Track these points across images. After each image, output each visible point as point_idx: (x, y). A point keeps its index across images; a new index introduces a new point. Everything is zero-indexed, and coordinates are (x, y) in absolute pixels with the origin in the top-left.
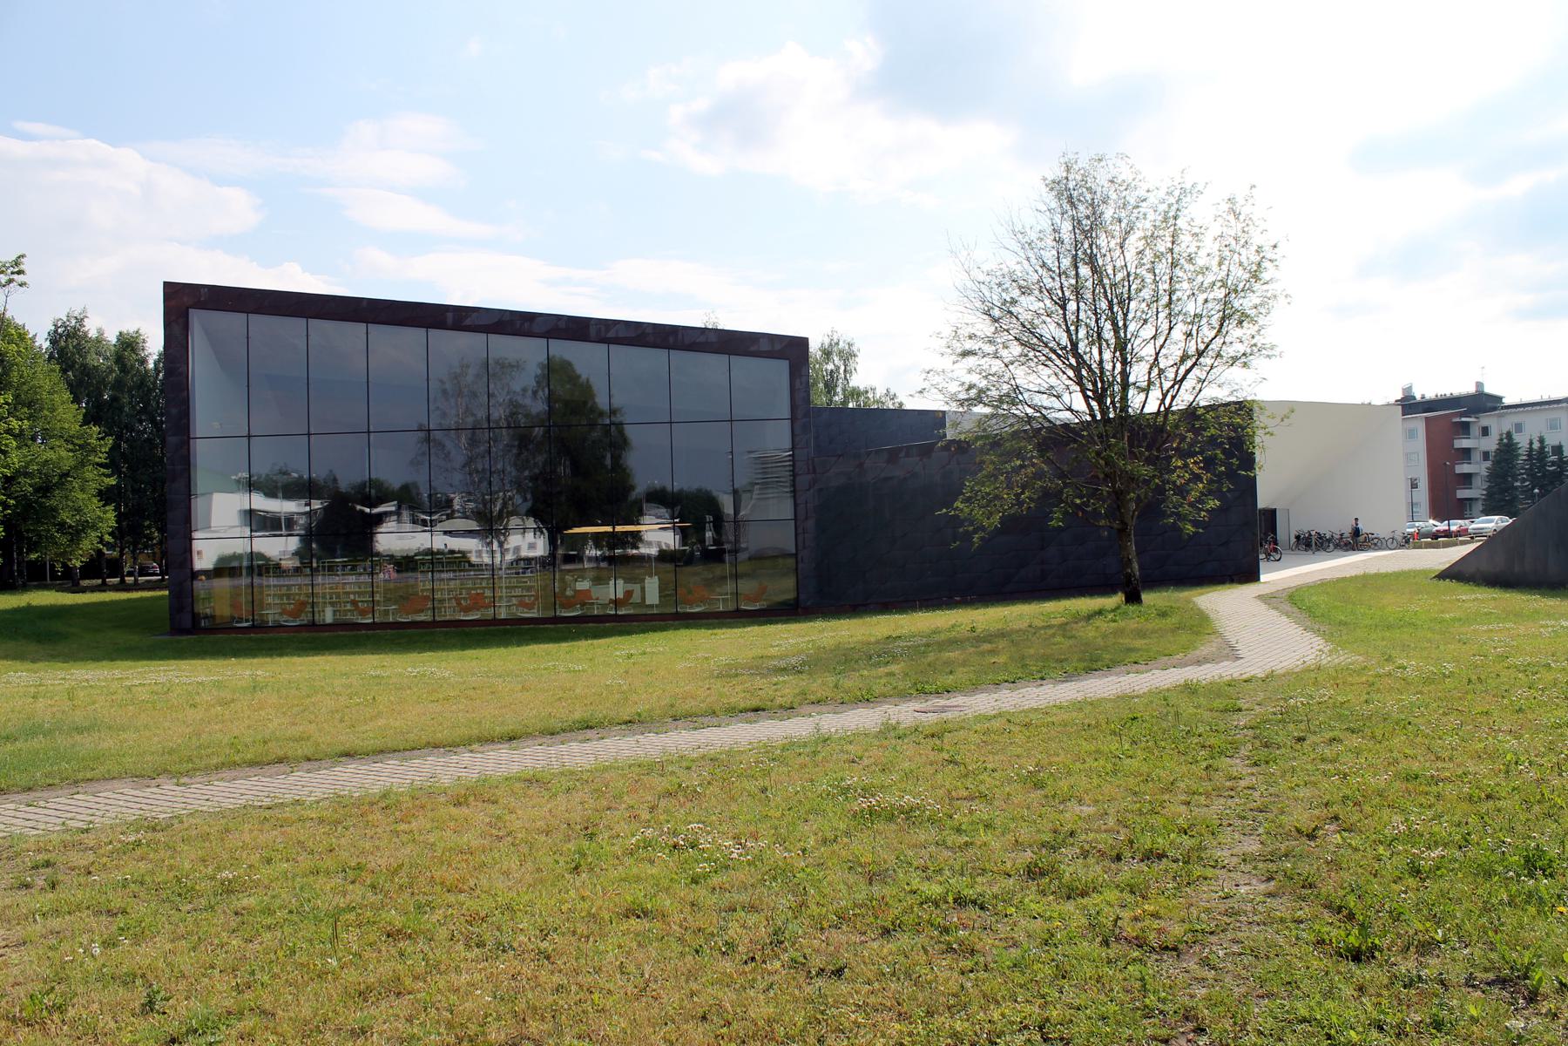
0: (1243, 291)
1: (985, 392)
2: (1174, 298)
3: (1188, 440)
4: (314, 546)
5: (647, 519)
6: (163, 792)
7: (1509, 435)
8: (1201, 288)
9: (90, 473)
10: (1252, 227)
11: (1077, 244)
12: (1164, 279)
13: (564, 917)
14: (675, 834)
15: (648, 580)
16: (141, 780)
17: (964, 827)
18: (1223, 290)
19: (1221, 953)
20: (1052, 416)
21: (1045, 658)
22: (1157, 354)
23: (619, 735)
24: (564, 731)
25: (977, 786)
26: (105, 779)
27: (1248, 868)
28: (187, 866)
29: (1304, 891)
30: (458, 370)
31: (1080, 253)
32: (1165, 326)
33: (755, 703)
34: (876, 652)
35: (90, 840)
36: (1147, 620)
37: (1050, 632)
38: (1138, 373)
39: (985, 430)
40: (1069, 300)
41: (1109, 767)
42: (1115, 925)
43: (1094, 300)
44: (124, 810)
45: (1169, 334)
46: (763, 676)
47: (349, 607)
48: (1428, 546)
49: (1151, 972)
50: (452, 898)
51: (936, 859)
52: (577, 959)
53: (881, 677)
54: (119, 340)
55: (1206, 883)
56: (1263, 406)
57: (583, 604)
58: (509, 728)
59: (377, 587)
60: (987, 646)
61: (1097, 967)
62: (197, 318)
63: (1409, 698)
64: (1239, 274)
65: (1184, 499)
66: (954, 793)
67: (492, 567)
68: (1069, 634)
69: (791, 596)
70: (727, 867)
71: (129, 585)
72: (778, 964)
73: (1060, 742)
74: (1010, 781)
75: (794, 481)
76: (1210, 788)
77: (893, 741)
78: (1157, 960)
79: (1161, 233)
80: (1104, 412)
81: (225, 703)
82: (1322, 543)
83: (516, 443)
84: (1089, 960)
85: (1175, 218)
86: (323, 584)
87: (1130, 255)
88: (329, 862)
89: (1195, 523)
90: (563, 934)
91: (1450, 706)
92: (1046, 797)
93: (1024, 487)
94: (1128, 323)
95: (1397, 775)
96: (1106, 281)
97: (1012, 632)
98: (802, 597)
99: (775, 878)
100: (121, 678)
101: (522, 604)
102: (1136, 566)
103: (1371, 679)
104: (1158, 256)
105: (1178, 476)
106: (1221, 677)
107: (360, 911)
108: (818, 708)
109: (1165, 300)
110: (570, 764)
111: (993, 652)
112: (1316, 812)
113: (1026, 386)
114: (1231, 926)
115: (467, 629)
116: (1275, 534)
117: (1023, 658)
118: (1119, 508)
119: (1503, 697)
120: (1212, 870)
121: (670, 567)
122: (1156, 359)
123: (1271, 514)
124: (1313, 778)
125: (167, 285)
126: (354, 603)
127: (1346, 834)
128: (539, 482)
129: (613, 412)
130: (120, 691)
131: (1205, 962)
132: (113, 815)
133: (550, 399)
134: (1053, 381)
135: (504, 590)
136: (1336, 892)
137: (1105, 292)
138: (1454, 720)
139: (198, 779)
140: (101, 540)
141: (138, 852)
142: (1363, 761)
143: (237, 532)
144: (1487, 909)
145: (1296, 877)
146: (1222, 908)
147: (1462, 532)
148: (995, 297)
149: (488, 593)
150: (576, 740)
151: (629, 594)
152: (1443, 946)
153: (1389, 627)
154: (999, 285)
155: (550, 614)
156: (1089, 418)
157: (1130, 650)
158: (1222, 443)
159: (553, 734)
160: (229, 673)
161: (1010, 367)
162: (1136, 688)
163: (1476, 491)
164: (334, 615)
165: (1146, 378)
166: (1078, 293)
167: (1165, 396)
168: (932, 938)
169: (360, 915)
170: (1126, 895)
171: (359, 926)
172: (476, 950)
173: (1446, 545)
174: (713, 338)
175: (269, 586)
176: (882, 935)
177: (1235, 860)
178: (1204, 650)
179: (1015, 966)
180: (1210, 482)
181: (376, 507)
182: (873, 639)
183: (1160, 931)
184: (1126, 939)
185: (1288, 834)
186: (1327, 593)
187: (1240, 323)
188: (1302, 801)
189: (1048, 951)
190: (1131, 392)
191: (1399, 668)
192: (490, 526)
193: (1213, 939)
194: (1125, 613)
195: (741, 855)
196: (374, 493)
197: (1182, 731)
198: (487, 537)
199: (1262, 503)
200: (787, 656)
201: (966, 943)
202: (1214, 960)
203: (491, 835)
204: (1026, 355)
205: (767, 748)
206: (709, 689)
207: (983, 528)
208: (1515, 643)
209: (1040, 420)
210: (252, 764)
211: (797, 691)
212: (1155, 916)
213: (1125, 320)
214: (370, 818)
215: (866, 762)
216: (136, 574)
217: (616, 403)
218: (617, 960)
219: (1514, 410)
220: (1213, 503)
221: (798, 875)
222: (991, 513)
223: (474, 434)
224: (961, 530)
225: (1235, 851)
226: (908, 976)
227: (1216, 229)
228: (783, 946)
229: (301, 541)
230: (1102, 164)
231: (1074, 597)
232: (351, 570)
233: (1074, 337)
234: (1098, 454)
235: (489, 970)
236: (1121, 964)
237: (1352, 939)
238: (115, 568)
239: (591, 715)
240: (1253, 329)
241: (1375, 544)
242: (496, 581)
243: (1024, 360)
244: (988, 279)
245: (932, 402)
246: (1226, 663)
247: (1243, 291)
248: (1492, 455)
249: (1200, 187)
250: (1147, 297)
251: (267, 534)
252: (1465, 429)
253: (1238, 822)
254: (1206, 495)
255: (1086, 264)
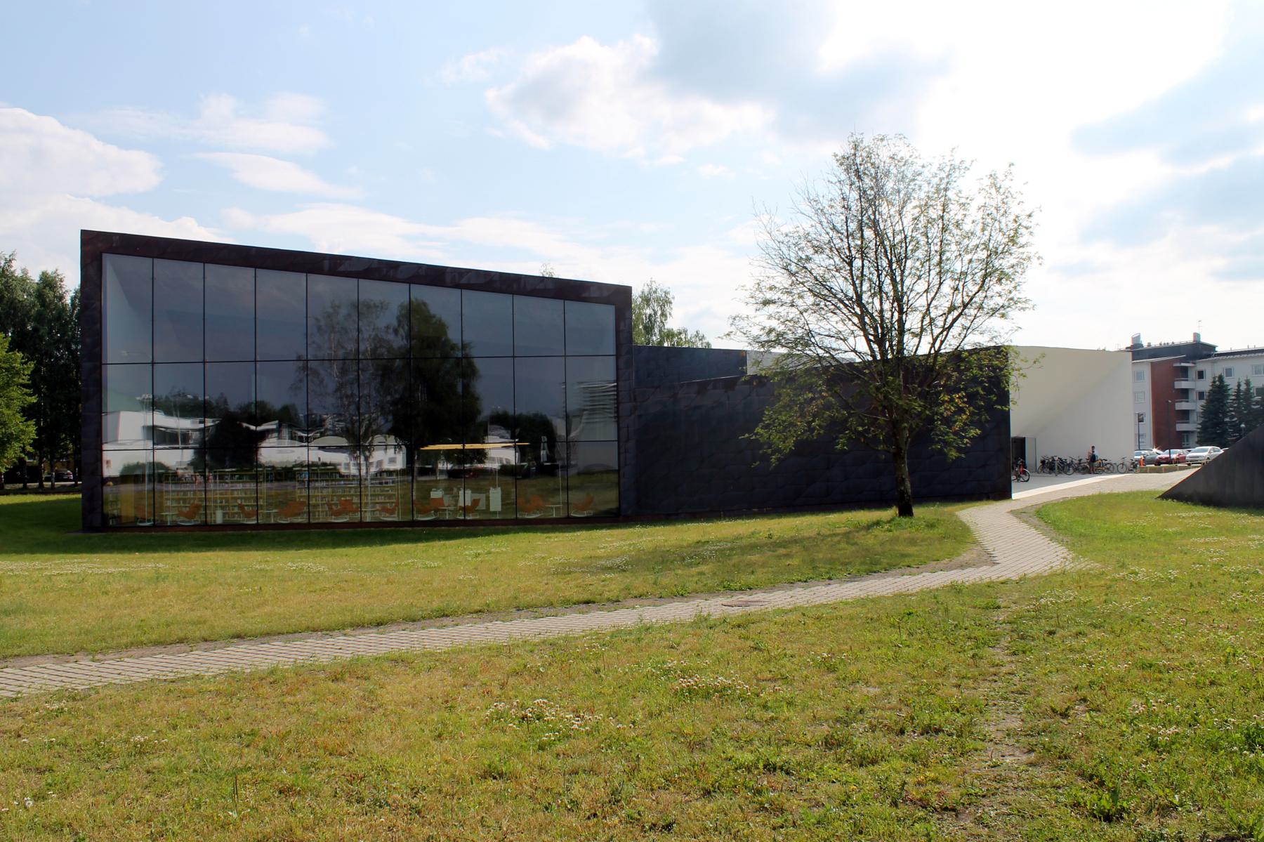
0: (1002, 253)
1: (782, 336)
2: (944, 258)
3: (954, 378)
4: (207, 458)
5: (490, 438)
6: (80, 666)
7: (1221, 378)
8: (967, 251)
9: (15, 393)
10: (1010, 199)
11: (863, 211)
12: (935, 241)
13: (431, 777)
14: (523, 707)
15: (492, 491)
16: (61, 657)
17: (769, 704)
18: (985, 251)
19: (993, 814)
20: (840, 356)
21: (831, 561)
22: (929, 305)
23: (471, 622)
24: (423, 618)
25: (779, 669)
26: (30, 655)
27: (1012, 741)
28: (104, 730)
29: (1060, 762)
30: (331, 310)
31: (864, 218)
32: (936, 281)
33: (586, 596)
34: (688, 555)
35: (19, 707)
36: (917, 530)
37: (836, 539)
38: (913, 322)
39: (782, 368)
40: (855, 258)
41: (891, 654)
42: (902, 789)
43: (877, 259)
44: (48, 682)
45: (939, 289)
46: (593, 573)
47: (236, 510)
48: (1152, 471)
49: (934, 829)
50: (334, 761)
51: (747, 731)
52: (444, 814)
53: (693, 576)
54: (41, 279)
55: (976, 753)
56: (1018, 350)
57: (437, 510)
58: (378, 615)
59: (261, 493)
60: (782, 551)
61: (888, 824)
62: (110, 262)
63: (1141, 599)
64: (1000, 238)
65: (950, 427)
66: (759, 676)
67: (360, 479)
68: (852, 541)
69: (614, 505)
70: (569, 737)
71: (47, 488)
72: (616, 820)
73: (847, 632)
74: (807, 666)
75: (618, 408)
76: (977, 673)
77: (706, 631)
78: (938, 819)
79: (933, 203)
80: (884, 353)
81: (132, 591)
82: (1063, 468)
83: (380, 372)
84: (881, 818)
85: (946, 190)
86: (215, 490)
87: (907, 220)
88: (226, 729)
89: (959, 450)
90: (431, 793)
91: (1176, 606)
92: (838, 679)
93: (814, 416)
94: (904, 278)
95: (1135, 664)
96: (887, 243)
97: (804, 539)
99: (610, 746)
100: (42, 569)
101: (385, 510)
102: (908, 484)
103: (1108, 583)
104: (930, 221)
105: (946, 409)
106: (981, 579)
107: (255, 771)
108: (640, 601)
109: (936, 259)
110: (430, 647)
111: (787, 556)
112: (1068, 695)
113: (817, 331)
114: (1000, 791)
115: (338, 531)
116: (1024, 459)
117: (813, 561)
118: (895, 435)
119: (1221, 599)
120: (981, 742)
121: (510, 479)
122: (928, 309)
123: (1021, 442)
124: (1064, 666)
125: (84, 233)
126: (241, 507)
127: (1093, 714)
128: (399, 406)
129: (464, 347)
130: (41, 580)
131: (979, 821)
132: (38, 687)
133: (410, 336)
134: (840, 327)
135: (369, 498)
136: (1087, 762)
137: (886, 251)
138: (1179, 618)
139: (111, 656)
140: (23, 450)
141: (61, 719)
142: (1105, 651)
143: (141, 445)
144: (1215, 778)
145: (1053, 749)
146: (992, 775)
147: (1180, 460)
148: (793, 255)
149: (356, 500)
150: (435, 627)
151: (475, 502)
152: (1180, 809)
153: (1122, 539)
154: (796, 244)
155: (409, 518)
156: (870, 359)
157: (904, 556)
158: (983, 381)
159: (414, 621)
160: (135, 566)
161: (805, 314)
162: (910, 588)
163: (1193, 425)
164: (224, 515)
165: (920, 325)
166: (863, 252)
167: (935, 341)
168: (746, 798)
169: (255, 774)
170: (910, 764)
171: (255, 784)
172: (356, 805)
173: (1167, 470)
174: (550, 286)
175: (167, 492)
176: (704, 795)
177: (1000, 735)
178: (966, 556)
179: (819, 822)
180: (972, 414)
181: (260, 425)
182: (685, 544)
183: (940, 794)
184: (911, 801)
185: (1044, 713)
186: (1069, 510)
187: (1000, 280)
188: (1055, 685)
189: (846, 811)
190: (907, 337)
191: (1132, 574)
192: (358, 444)
193: (985, 801)
194: (899, 524)
195: (580, 726)
196: (260, 413)
197: (951, 624)
198: (355, 452)
199: (1015, 432)
200: (612, 557)
201: (776, 803)
202: (987, 820)
203: (366, 707)
204: (818, 305)
205: (598, 635)
206: (547, 584)
207: (779, 450)
208: (1228, 554)
209: (829, 359)
210: (157, 643)
211: (622, 587)
212: (936, 781)
213: (902, 275)
214: (261, 691)
215: (683, 648)
216: (53, 480)
217: (467, 338)
218: (478, 815)
219: (1225, 357)
220: (974, 432)
221: (630, 744)
222: (786, 438)
223: (344, 364)
224: (761, 452)
225: (1000, 727)
226: (728, 830)
227: (979, 200)
228: (619, 804)
229: (195, 453)
230: (885, 143)
231: (855, 510)
232: (240, 478)
233: (859, 289)
234: (878, 389)
235: (369, 823)
236: (909, 822)
237: (1104, 802)
238: (35, 474)
239: (447, 605)
240: (1010, 286)
241: (1108, 469)
242: (363, 489)
243: (816, 308)
244: (786, 239)
245: (737, 343)
246: (985, 568)
247: (1002, 253)
248: (1206, 395)
249: (967, 164)
250: (921, 256)
251: (167, 447)
252: (1184, 372)
253: (1002, 703)
254: (968, 425)
255: (870, 228)
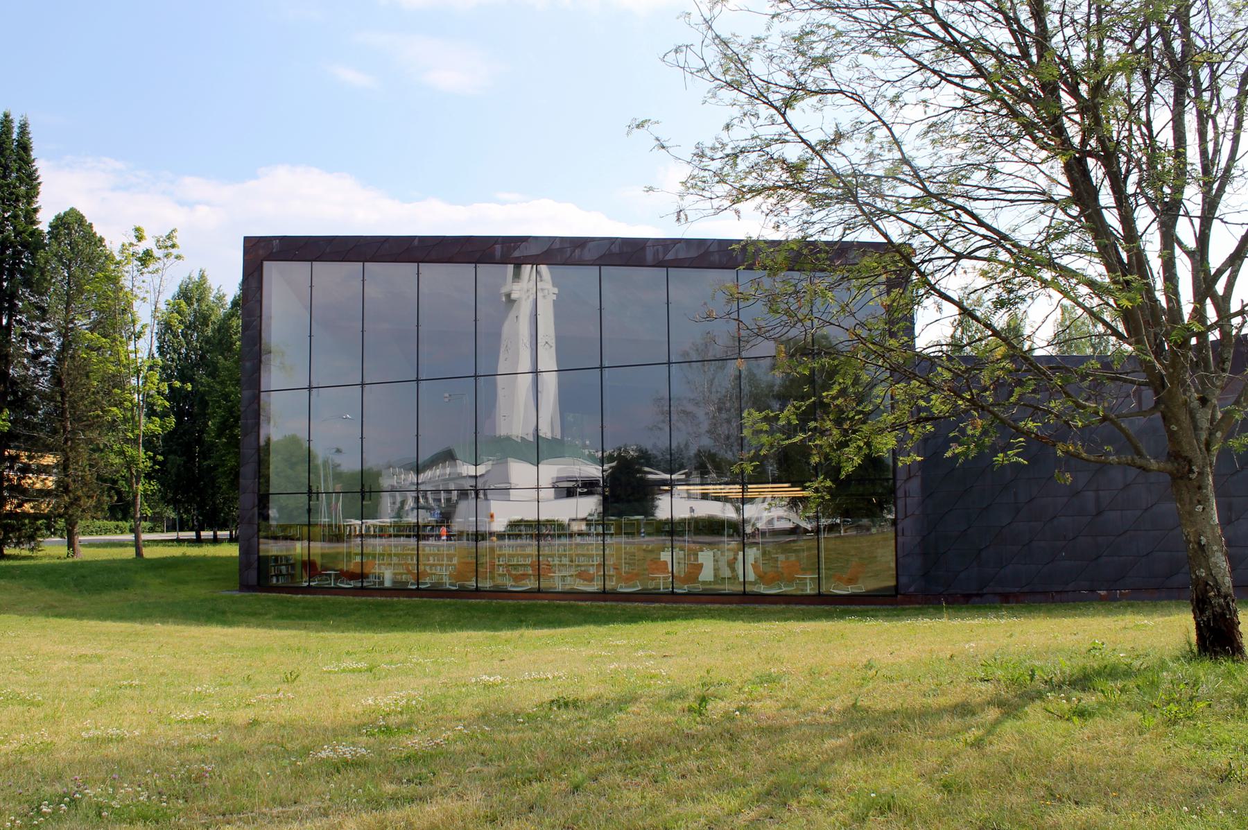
98: (903, 580)
